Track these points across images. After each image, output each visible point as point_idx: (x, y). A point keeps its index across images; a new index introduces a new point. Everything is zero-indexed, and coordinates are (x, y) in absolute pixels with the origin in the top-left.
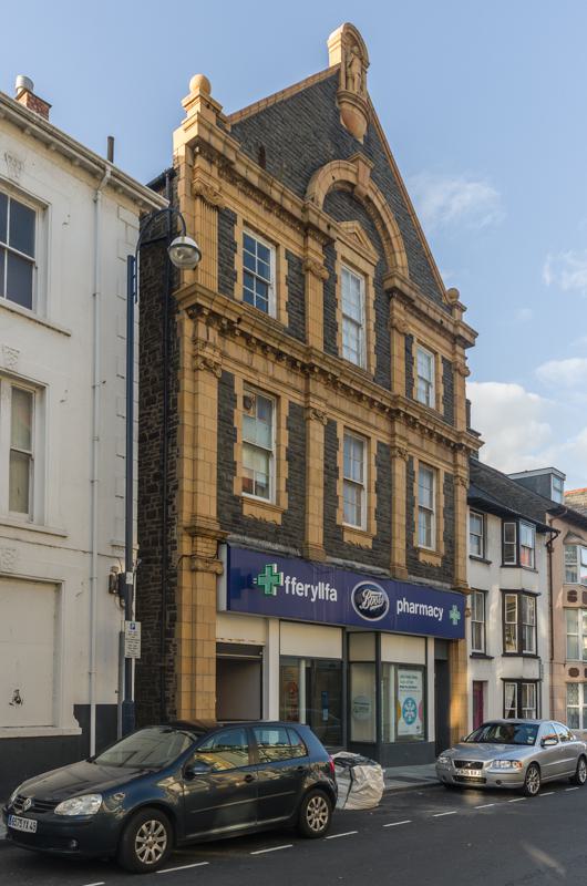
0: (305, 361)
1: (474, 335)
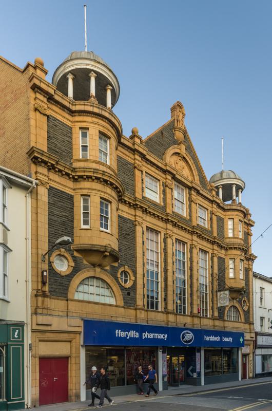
1: (254, 223)
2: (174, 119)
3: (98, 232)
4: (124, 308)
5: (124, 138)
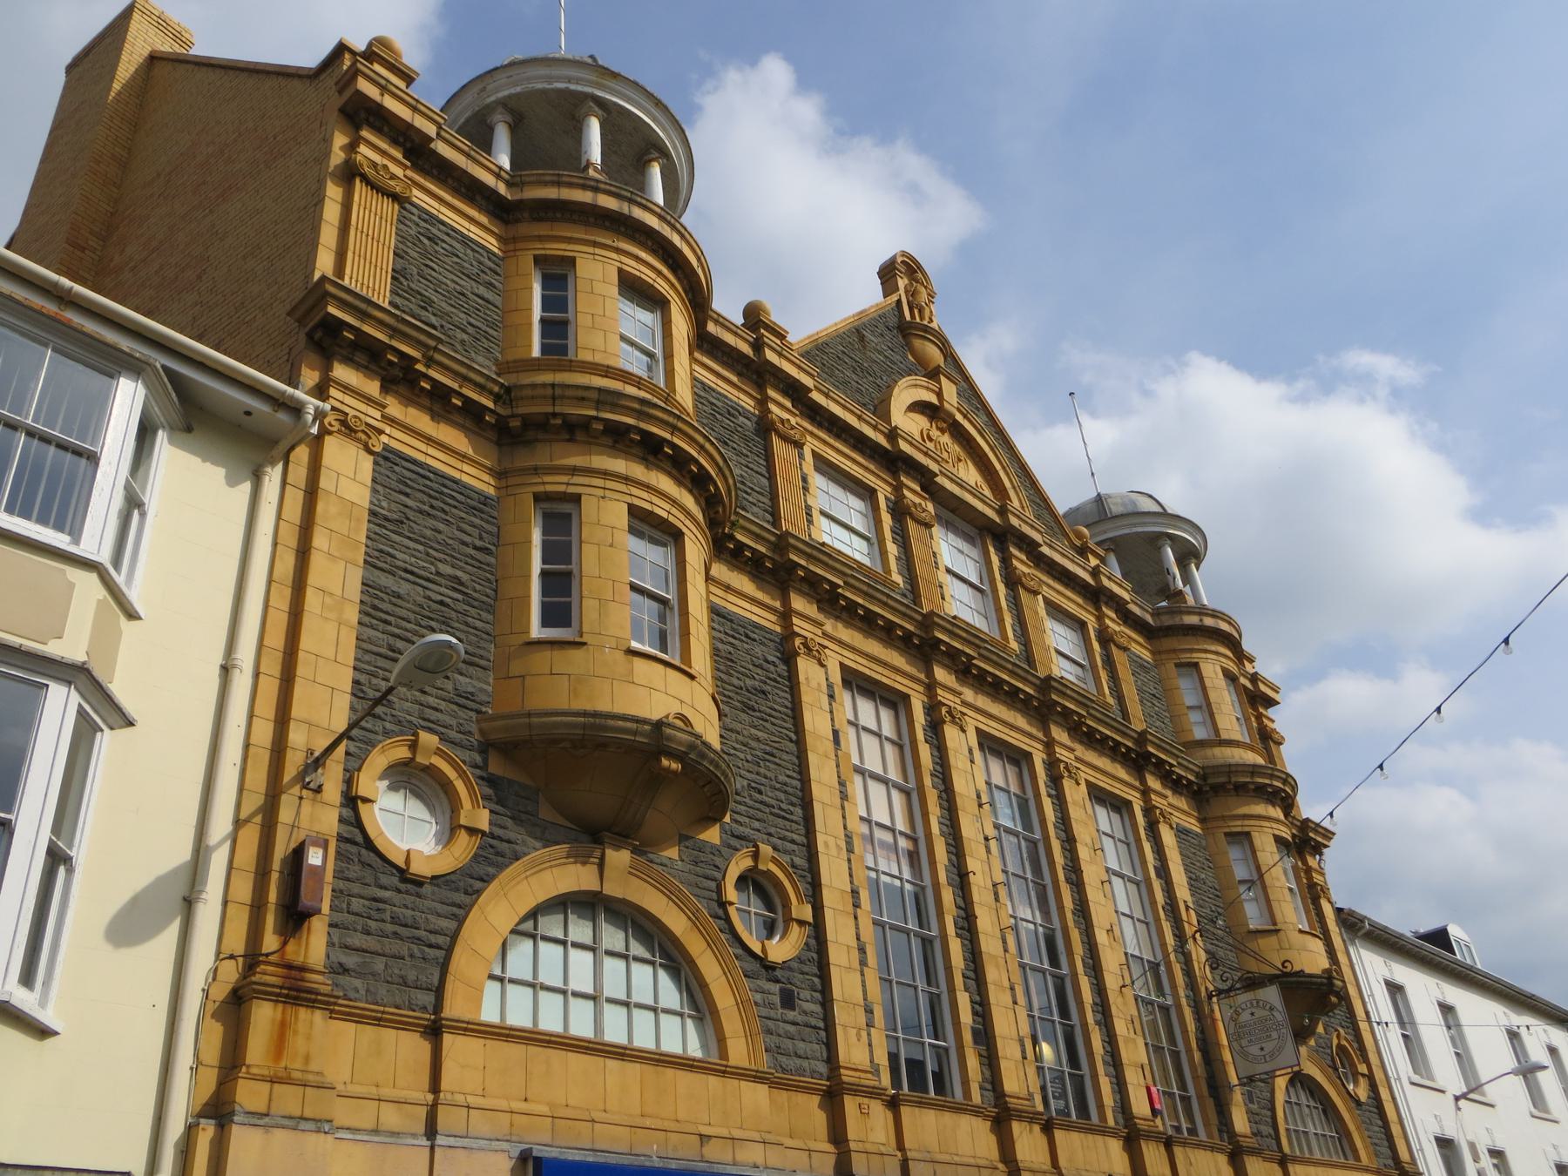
3: (620, 655)
4: (774, 1084)
5: (717, 322)
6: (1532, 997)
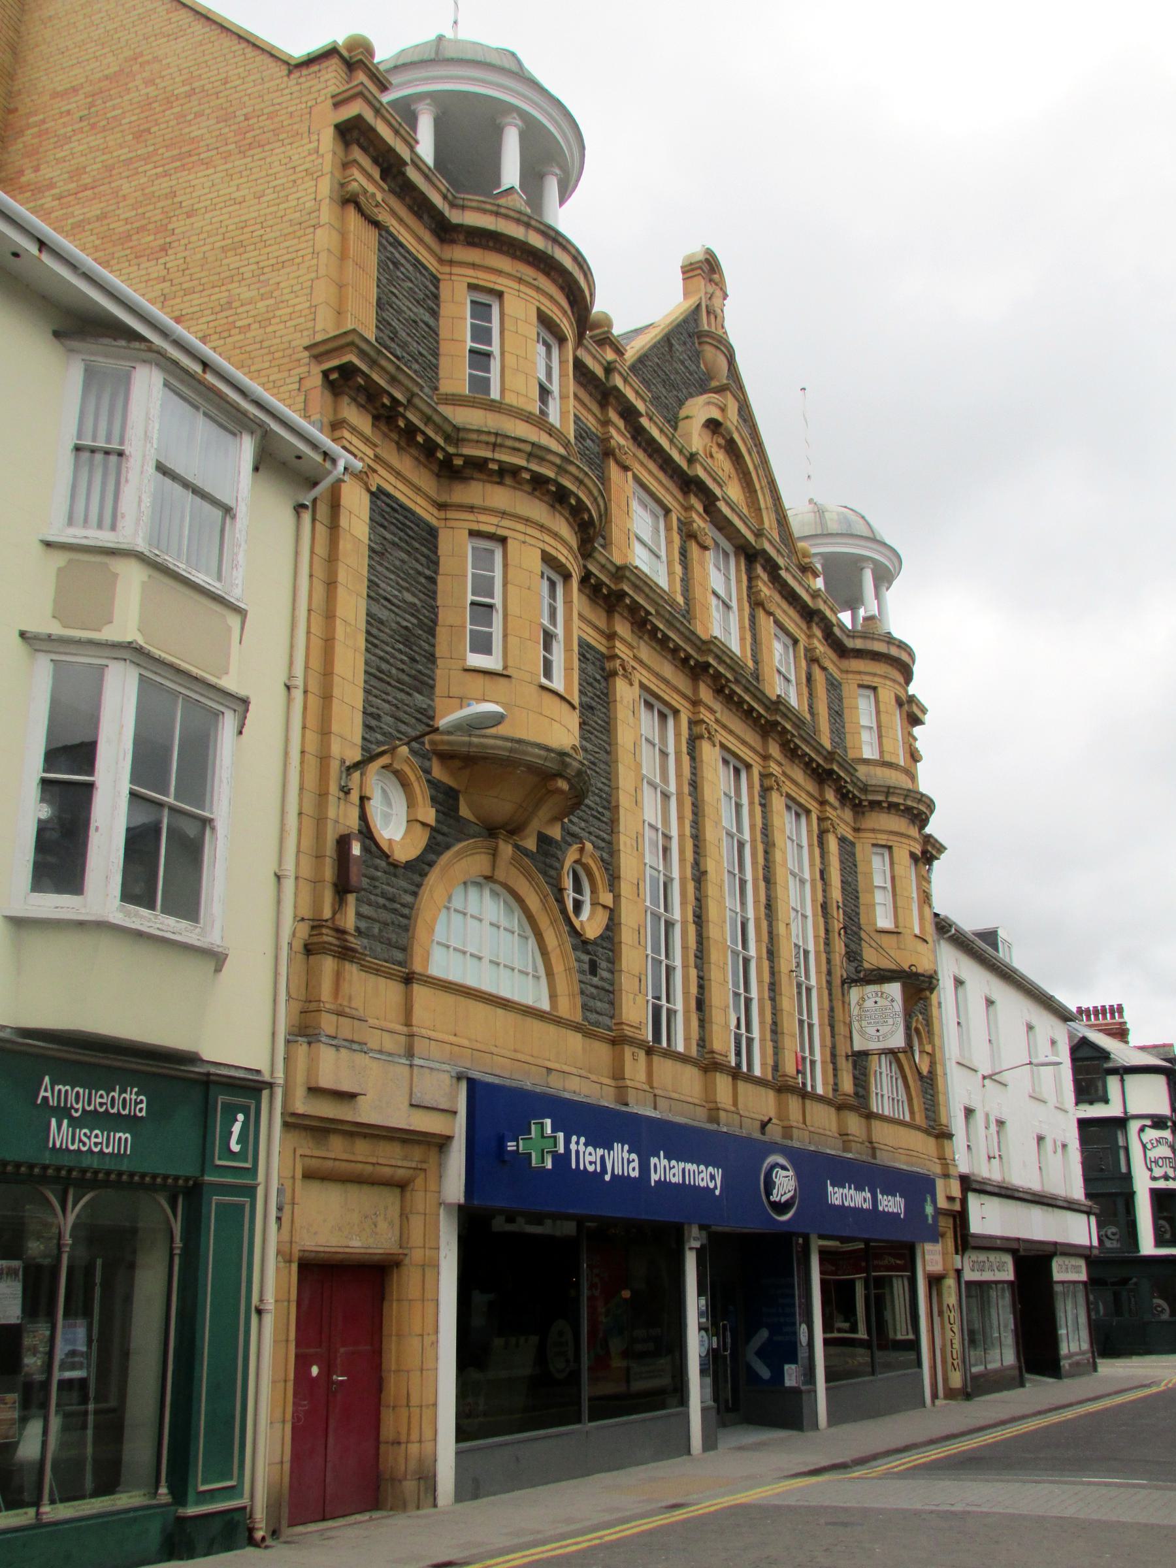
0: (613, 586)
2: (699, 306)
3: (534, 689)
4: (587, 1034)
6: (1051, 998)
